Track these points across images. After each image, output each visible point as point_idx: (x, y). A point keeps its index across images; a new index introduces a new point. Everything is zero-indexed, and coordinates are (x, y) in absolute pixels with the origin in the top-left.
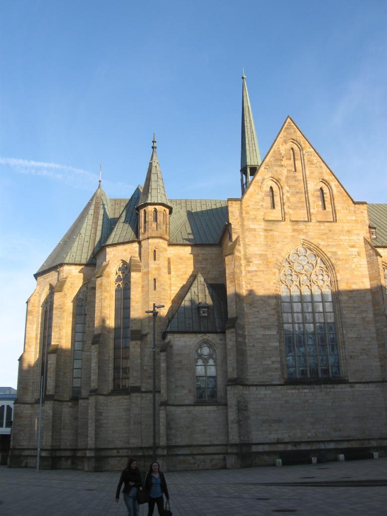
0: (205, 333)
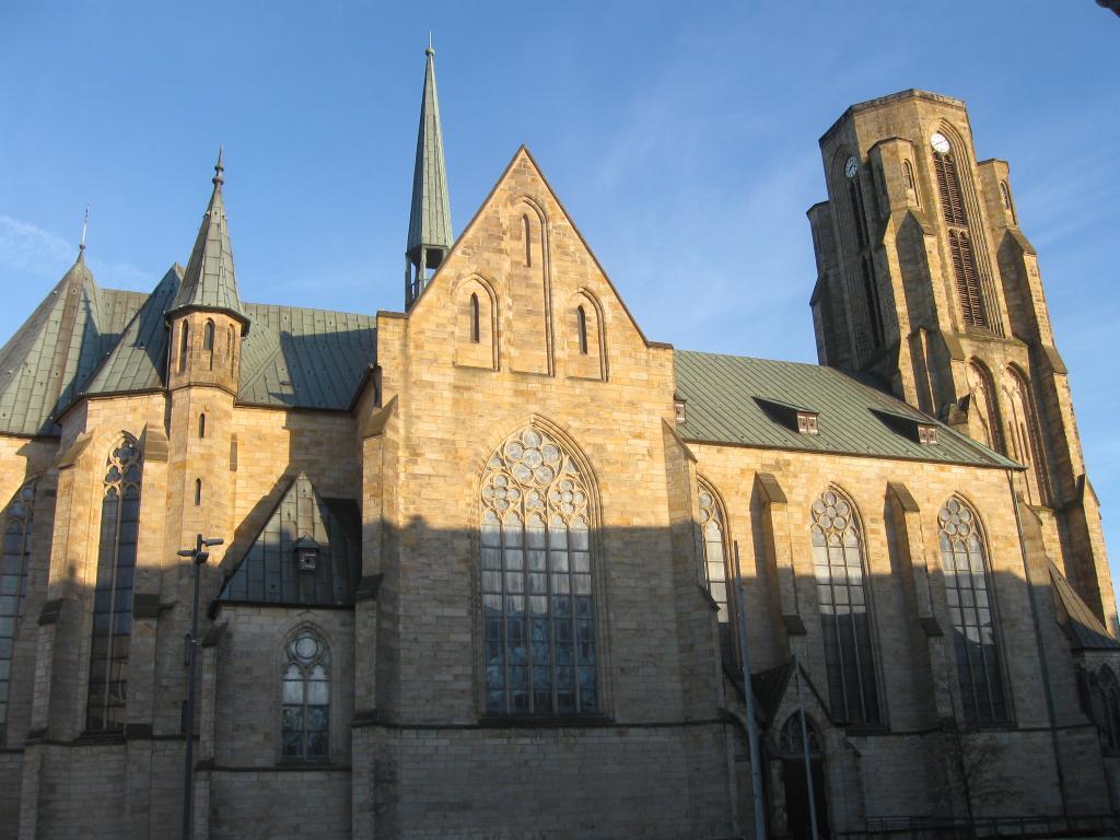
0: (307, 607)
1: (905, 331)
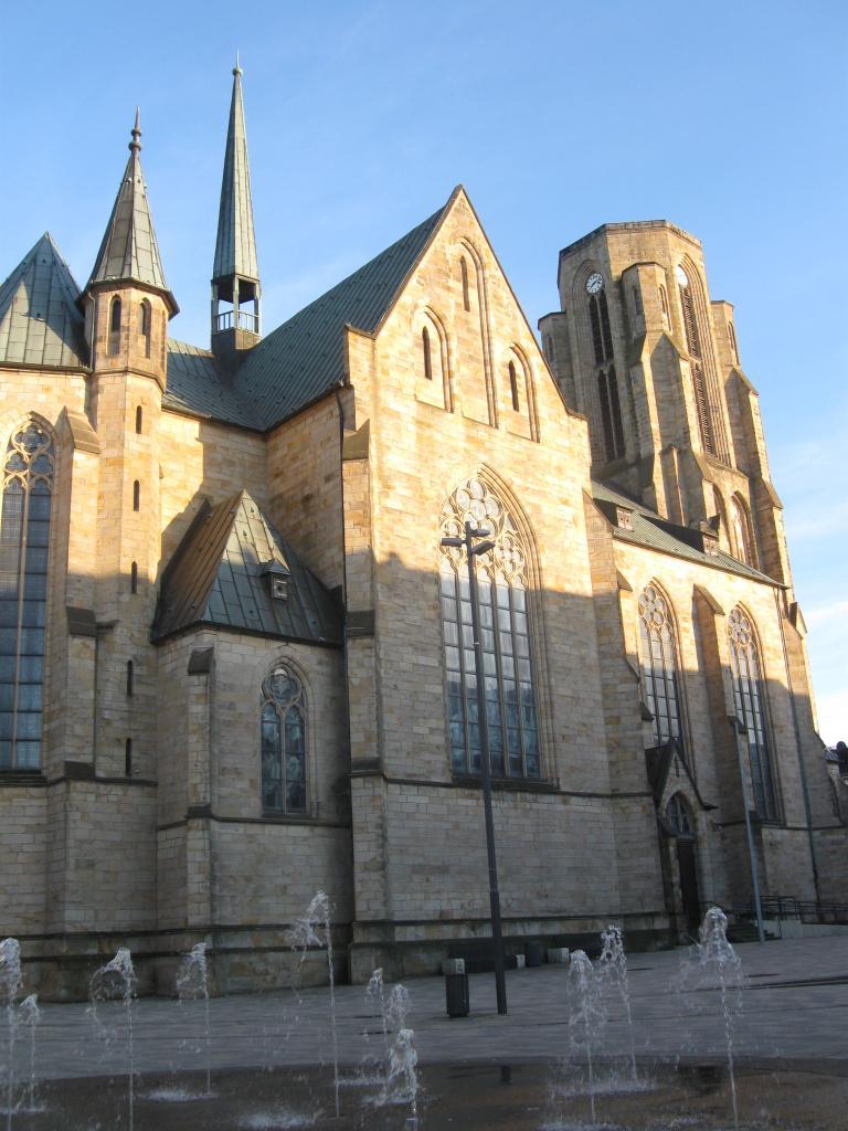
0: (287, 639)
1: (658, 448)
